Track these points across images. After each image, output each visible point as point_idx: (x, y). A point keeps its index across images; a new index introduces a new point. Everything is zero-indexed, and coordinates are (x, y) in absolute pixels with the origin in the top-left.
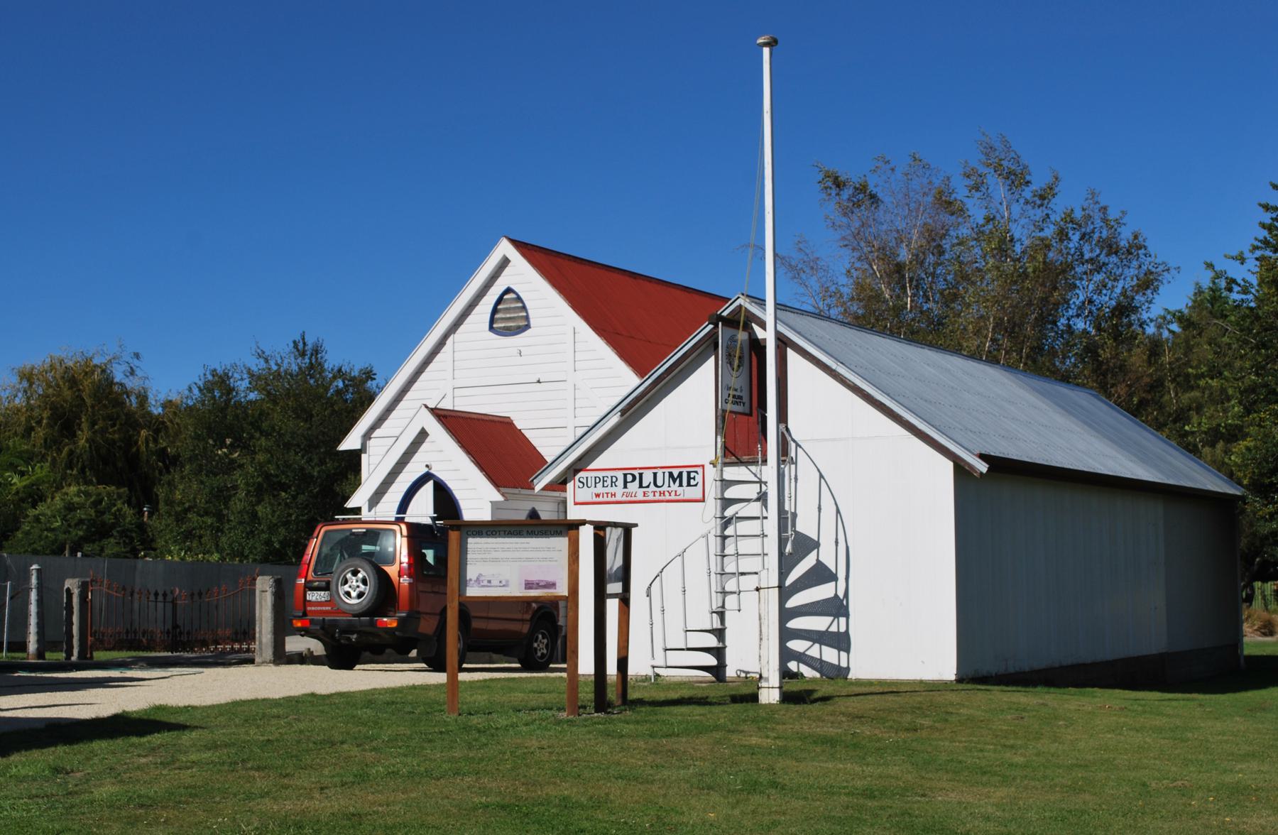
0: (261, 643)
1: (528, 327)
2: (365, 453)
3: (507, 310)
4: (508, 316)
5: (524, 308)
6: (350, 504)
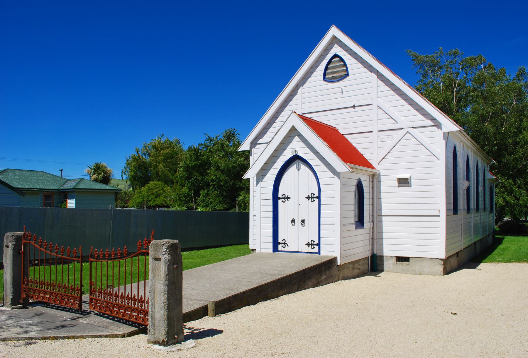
0: (153, 318)
1: (347, 75)
2: (251, 156)
3: (334, 67)
4: (335, 70)
5: (345, 65)
6: (245, 177)
